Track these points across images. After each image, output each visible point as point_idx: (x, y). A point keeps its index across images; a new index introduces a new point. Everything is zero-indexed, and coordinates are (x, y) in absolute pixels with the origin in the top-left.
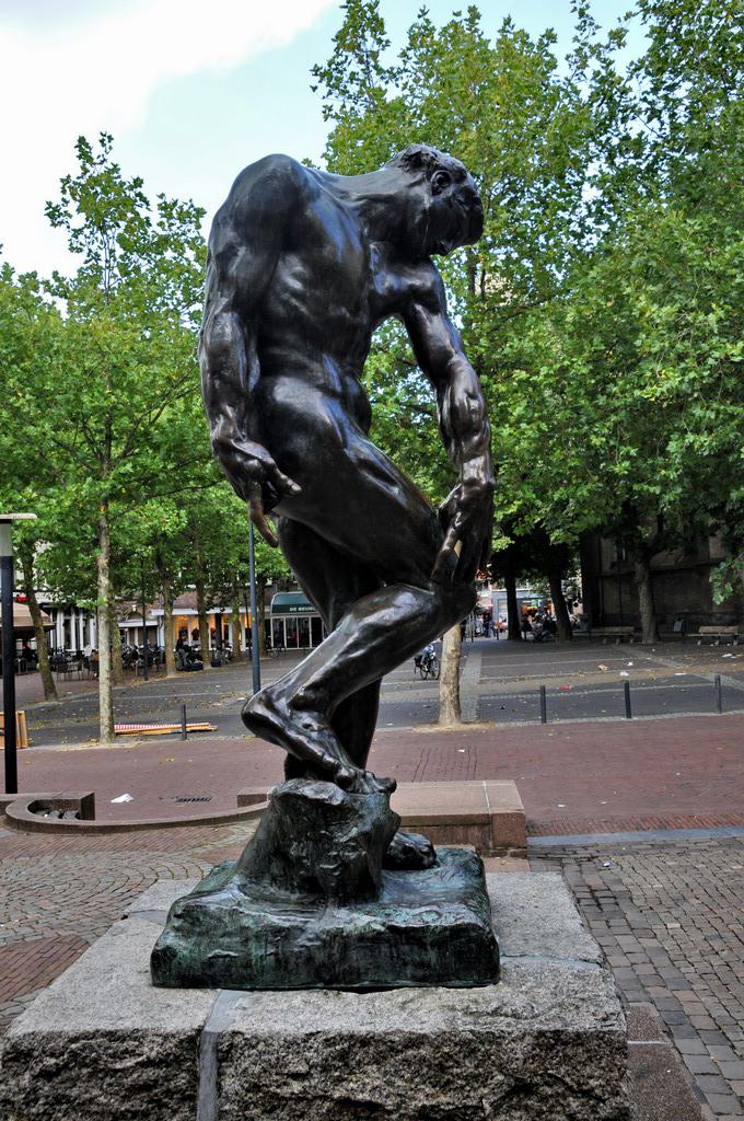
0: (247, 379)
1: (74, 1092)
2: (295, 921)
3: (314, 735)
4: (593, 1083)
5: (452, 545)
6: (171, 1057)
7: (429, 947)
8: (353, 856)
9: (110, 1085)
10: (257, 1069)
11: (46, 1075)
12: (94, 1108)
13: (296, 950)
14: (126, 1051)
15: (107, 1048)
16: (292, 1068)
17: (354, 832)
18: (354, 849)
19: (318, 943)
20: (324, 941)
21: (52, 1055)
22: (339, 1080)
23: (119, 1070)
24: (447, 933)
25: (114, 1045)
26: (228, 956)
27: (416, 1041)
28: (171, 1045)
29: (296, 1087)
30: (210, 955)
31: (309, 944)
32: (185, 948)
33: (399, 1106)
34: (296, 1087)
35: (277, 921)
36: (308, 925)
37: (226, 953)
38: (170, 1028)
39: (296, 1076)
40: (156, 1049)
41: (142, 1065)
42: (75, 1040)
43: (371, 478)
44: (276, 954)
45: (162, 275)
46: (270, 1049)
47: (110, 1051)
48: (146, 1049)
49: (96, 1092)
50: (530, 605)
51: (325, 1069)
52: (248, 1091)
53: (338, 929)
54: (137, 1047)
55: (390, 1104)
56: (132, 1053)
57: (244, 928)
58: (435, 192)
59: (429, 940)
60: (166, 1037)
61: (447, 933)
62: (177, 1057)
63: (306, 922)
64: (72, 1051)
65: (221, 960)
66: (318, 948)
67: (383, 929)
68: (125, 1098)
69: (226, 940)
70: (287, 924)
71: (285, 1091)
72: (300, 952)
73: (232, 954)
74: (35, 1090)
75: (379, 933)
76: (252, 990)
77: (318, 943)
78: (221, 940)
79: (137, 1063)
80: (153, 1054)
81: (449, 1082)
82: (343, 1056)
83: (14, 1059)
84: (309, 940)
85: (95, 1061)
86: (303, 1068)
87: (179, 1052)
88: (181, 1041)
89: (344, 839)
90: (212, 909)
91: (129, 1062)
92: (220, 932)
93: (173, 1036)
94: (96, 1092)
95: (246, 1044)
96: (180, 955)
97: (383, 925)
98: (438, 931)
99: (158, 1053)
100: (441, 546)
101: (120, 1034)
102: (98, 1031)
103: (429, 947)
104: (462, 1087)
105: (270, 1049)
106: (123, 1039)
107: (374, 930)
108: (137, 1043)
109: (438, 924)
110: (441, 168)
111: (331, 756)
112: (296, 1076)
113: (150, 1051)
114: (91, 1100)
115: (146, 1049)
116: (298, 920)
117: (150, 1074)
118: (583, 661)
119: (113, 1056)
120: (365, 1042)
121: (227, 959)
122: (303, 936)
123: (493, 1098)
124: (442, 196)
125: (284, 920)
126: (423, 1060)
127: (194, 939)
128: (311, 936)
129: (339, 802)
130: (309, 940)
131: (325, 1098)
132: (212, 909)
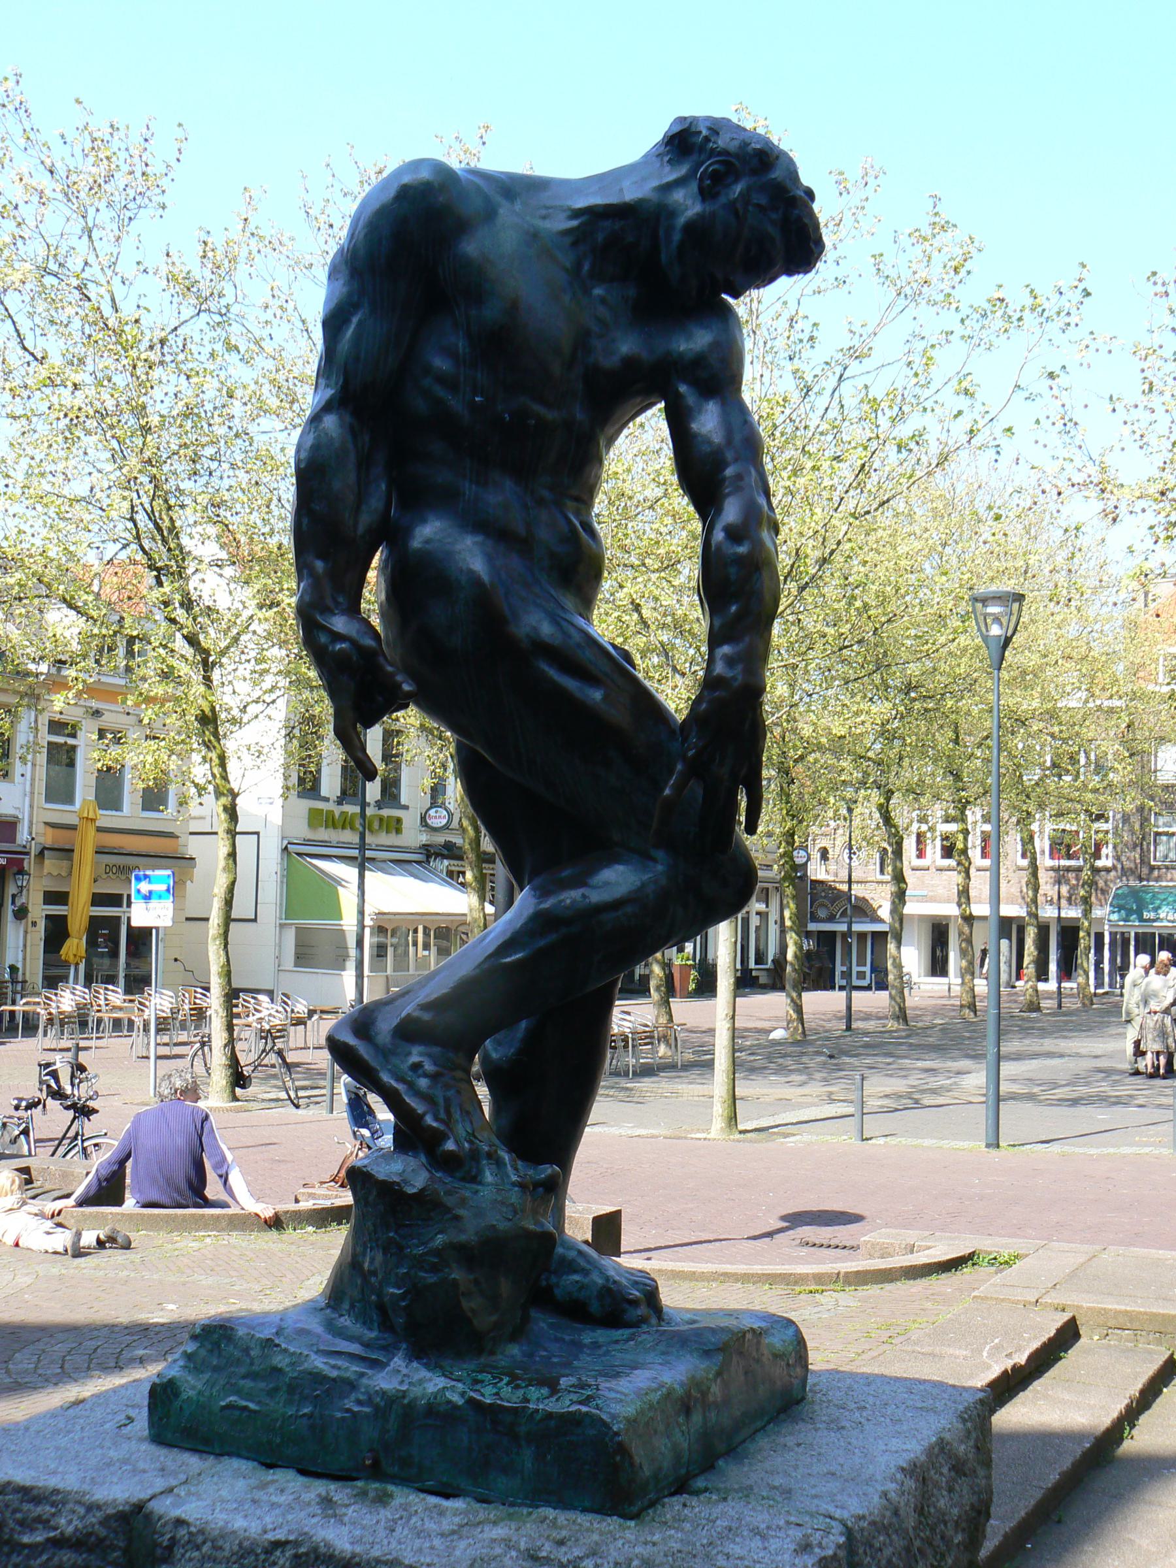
0: (357, 510)
2: (347, 1369)
3: (423, 1083)
5: (679, 788)
6: (93, 1539)
7: (523, 1443)
8: (431, 1279)
13: (339, 1415)
14: (39, 1520)
15: (15, 1511)
17: (440, 1239)
18: (434, 1269)
19: (367, 1410)
20: (376, 1408)
23: (25, 1546)
24: (553, 1423)
25: (26, 1507)
26: (245, 1408)
28: (94, 1520)
30: (223, 1403)
31: (356, 1409)
32: (193, 1388)
35: (321, 1366)
36: (364, 1381)
37: (244, 1403)
38: (100, 1495)
40: (75, 1523)
43: (553, 673)
44: (310, 1416)
46: (219, 1554)
47: (19, 1516)
48: (63, 1521)
53: (398, 1391)
54: (54, 1515)
57: (277, 1371)
58: (706, 194)
59: (523, 1430)
60: (91, 1508)
61: (553, 1423)
62: (101, 1541)
63: (362, 1375)
65: (237, 1413)
66: (367, 1416)
67: (461, 1402)
69: (248, 1384)
70: (334, 1374)
72: (343, 1419)
73: (252, 1406)
75: (455, 1407)
77: (367, 1410)
78: (242, 1382)
79: (48, 1540)
80: (70, 1529)
84: (359, 1402)
87: (103, 1533)
88: (108, 1518)
89: (421, 1250)
90: (240, 1333)
91: (39, 1537)
93: (99, 1507)
95: (189, 1542)
96: (184, 1396)
97: (463, 1394)
98: (538, 1417)
99: (76, 1529)
100: (662, 790)
101: (35, 1492)
102: (9, 1483)
103: (523, 1443)
105: (219, 1554)
107: (449, 1402)
108: (53, 1510)
109: (541, 1407)
110: (719, 154)
111: (436, 1119)
113: (67, 1524)
115: (63, 1521)
116: (352, 1369)
119: (21, 1523)
121: (245, 1414)
122: (353, 1397)
124: (723, 200)
125: (334, 1367)
127: (206, 1376)
128: (361, 1397)
129: (415, 1191)
132: (240, 1333)
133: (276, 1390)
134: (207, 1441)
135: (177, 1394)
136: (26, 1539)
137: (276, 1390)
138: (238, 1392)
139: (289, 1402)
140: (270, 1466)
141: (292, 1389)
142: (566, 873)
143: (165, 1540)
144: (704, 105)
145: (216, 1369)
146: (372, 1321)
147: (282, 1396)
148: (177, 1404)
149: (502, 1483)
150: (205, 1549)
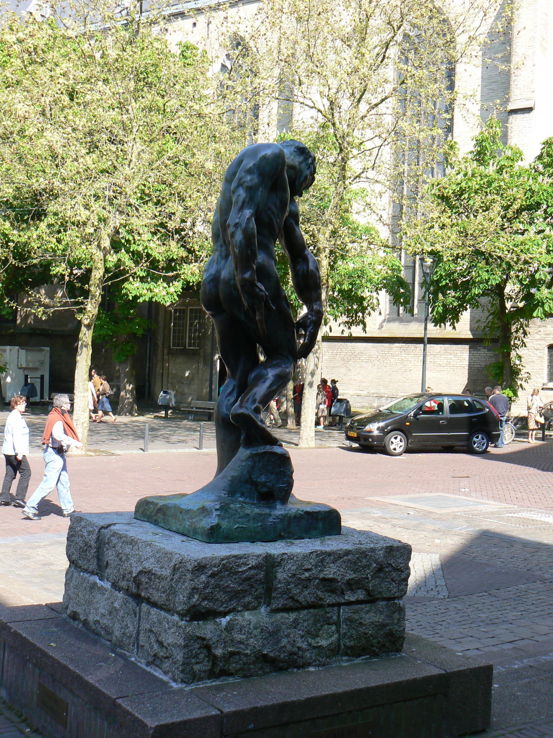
1: (222, 583)
4: (401, 565)
9: (235, 579)
10: (294, 568)
11: (213, 575)
12: (228, 589)
16: (306, 567)
20: (281, 519)
21: (215, 566)
22: (321, 571)
27: (348, 553)
29: (307, 574)
33: (341, 579)
34: (307, 574)
39: (307, 570)
41: (250, 569)
42: (222, 560)
45: (92, 230)
49: (230, 582)
50: (323, 410)
51: (316, 566)
52: (290, 577)
55: (339, 578)
56: (245, 564)
59: (319, 517)
64: (223, 564)
68: (241, 584)
71: (303, 577)
74: (208, 582)
76: (238, 542)
81: (357, 569)
82: (322, 560)
83: (197, 570)
84: (274, 519)
85: (231, 568)
86: (310, 567)
92: (237, 516)
94: (230, 582)
104: (361, 571)
106: (240, 558)
112: (307, 570)
114: (227, 586)
117: (253, 572)
118: (428, 494)
120: (329, 554)
123: (371, 574)
126: (349, 560)
130: (274, 519)
131: (316, 578)
133: (249, 520)
134: (232, 539)
135: (221, 527)
136: (240, 570)
137: (249, 520)
138: (238, 523)
139: (254, 523)
140: (253, 542)
141: (254, 519)
142: (274, 363)
143: (279, 560)
144: (544, 140)
145: (229, 518)
146: (254, 497)
147: (252, 522)
148: (222, 530)
149: (314, 532)
150: (295, 559)
